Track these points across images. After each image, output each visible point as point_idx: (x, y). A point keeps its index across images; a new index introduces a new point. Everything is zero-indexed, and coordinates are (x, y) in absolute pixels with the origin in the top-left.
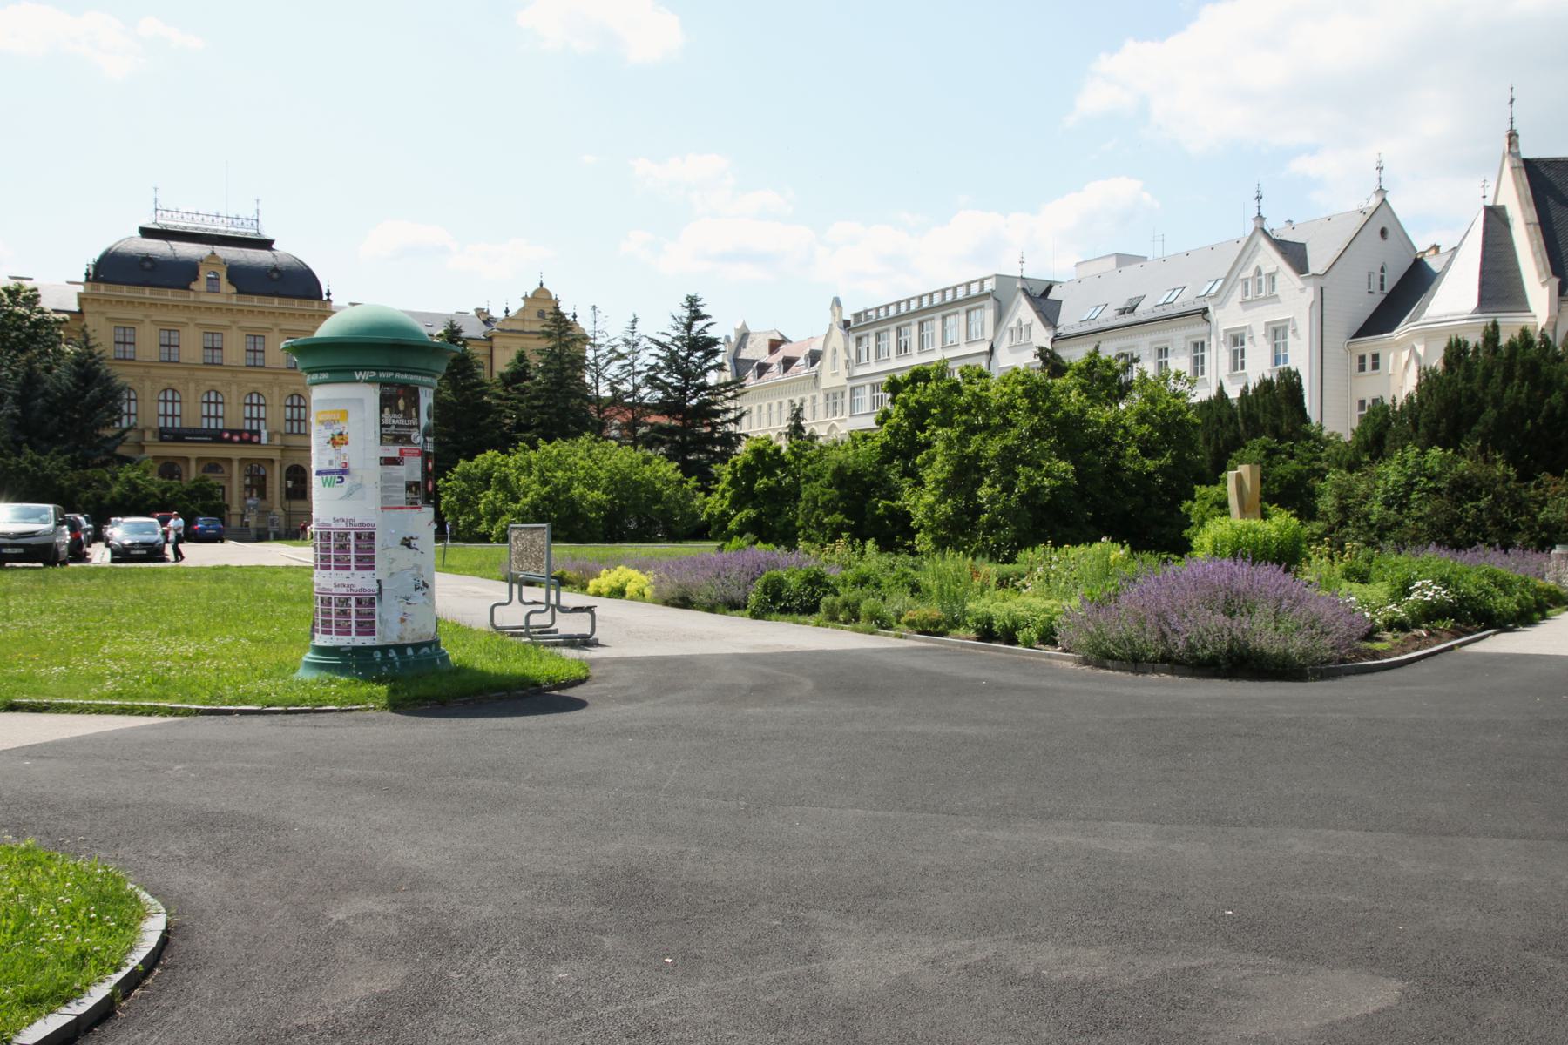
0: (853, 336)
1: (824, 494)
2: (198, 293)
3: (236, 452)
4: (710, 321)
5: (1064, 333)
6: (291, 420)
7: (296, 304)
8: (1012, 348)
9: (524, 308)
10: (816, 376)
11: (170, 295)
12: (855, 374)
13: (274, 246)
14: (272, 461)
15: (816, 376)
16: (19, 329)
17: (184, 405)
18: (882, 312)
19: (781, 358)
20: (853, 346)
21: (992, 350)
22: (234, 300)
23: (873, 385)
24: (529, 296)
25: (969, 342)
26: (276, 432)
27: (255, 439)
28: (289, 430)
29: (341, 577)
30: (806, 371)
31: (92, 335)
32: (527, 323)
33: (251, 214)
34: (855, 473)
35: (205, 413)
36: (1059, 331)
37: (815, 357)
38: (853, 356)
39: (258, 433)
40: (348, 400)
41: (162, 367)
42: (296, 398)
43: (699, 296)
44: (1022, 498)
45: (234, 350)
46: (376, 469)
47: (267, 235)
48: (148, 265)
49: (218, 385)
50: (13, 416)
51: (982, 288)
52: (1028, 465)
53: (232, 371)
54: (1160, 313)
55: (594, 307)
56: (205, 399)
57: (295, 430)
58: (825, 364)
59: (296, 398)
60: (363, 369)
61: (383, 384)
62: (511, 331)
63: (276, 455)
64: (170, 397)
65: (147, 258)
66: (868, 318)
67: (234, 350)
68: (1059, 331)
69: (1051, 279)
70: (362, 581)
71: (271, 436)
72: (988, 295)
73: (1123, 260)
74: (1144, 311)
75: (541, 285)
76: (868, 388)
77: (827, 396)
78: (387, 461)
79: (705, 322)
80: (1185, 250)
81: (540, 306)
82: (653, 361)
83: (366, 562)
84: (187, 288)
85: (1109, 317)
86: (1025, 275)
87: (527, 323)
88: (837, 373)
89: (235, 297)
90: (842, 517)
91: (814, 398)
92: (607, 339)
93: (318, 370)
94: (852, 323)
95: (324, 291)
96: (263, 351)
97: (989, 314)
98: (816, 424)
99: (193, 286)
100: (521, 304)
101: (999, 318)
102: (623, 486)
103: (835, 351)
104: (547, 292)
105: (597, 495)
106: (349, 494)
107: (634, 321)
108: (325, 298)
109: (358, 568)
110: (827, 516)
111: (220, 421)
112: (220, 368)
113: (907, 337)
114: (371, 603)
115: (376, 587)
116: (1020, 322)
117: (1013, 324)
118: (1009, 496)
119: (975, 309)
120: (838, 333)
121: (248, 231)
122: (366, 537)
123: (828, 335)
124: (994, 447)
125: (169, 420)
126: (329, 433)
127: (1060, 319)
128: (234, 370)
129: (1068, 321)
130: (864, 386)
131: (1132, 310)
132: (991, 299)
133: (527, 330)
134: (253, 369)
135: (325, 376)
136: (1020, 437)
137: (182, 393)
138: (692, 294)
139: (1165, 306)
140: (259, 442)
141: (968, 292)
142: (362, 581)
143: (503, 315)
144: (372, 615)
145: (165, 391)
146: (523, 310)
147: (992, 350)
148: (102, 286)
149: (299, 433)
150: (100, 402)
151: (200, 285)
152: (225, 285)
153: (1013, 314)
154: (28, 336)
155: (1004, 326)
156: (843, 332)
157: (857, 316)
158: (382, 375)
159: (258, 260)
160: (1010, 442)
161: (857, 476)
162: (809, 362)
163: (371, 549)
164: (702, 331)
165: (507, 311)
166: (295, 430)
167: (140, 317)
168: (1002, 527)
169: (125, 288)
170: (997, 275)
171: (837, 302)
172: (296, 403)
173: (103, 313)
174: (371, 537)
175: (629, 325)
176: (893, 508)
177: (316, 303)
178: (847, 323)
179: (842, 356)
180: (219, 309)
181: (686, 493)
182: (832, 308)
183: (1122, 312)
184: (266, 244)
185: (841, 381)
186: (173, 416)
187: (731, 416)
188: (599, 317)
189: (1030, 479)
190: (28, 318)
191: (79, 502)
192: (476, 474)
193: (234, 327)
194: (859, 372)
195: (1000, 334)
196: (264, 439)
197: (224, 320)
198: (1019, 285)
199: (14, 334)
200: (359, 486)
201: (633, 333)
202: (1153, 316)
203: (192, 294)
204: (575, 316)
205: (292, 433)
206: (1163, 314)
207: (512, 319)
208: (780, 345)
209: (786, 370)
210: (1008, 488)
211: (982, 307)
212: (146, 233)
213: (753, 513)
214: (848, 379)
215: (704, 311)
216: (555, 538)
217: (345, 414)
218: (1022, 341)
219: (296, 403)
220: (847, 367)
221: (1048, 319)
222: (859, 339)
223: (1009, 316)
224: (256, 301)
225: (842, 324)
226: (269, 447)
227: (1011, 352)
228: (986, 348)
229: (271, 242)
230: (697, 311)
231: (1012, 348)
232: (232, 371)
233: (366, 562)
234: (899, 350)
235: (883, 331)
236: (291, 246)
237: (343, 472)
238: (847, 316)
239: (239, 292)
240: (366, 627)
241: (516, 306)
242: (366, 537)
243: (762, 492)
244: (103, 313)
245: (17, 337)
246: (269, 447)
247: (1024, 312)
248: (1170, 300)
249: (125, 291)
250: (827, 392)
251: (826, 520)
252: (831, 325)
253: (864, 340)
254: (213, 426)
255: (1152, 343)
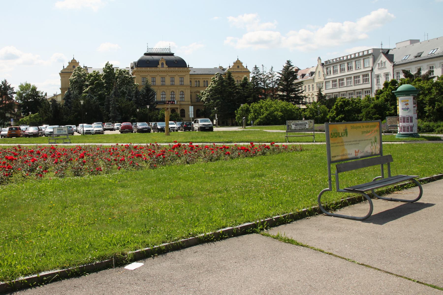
0: (325, 68)
1: (372, 110)
2: (159, 68)
3: (169, 106)
4: (293, 67)
5: (397, 64)
6: (181, 98)
7: (181, 69)
8: (379, 69)
9: (234, 65)
10: (313, 79)
11: (153, 69)
12: (326, 78)
13: (174, 55)
14: (177, 108)
15: (313, 79)
16: (127, 80)
17: (166, 95)
18: (334, 60)
19: (301, 74)
20: (325, 70)
21: (372, 70)
22: (167, 69)
23: (332, 81)
24: (70, 62)
25: (364, 67)
26: (179, 101)
27: (174, 103)
28: (180, 100)
29: (408, 124)
30: (310, 78)
31: (148, 80)
32: (235, 69)
33: (168, 47)
34: (380, 105)
35: (162, 97)
36: (395, 63)
37: (312, 74)
38: (325, 73)
39: (174, 101)
40: (409, 99)
41: (162, 86)
42: (182, 92)
43: (290, 60)
44: (437, 109)
45: (168, 81)
46: (413, 108)
47: (172, 52)
48: (148, 62)
49: (164, 90)
50: (135, 100)
51: (368, 53)
52: (438, 102)
53: (186, 86)
54: (430, 56)
55: (263, 65)
56: (180, 94)
57: (182, 100)
58: (316, 76)
59: (182, 92)
60: (411, 94)
61: (413, 96)
62: (65, 72)
63: (178, 107)
64: (173, 93)
65: (148, 61)
66: (330, 62)
67: (168, 81)
68: (395, 63)
69: (389, 48)
70: (411, 124)
71: (177, 102)
72: (370, 54)
73: (413, 42)
74: (423, 56)
75: (238, 59)
76: (331, 82)
77: (317, 84)
78: (414, 107)
79: (292, 67)
80: (437, 37)
81: (238, 65)
82: (277, 78)
83: (411, 121)
84: (157, 67)
85: (412, 58)
86: (383, 48)
87: (235, 69)
88: (320, 78)
89: (167, 68)
90: (378, 116)
91: (313, 85)
92: (266, 73)
93: (399, 95)
94: (325, 64)
95: (187, 65)
96: (183, 81)
97: (371, 60)
98: (314, 92)
99: (158, 66)
100: (68, 64)
101: (374, 61)
102: (284, 110)
103: (319, 72)
104: (240, 61)
105: (280, 114)
106: (409, 112)
107: (272, 68)
108: (188, 67)
109: (410, 122)
110: (373, 115)
111: (165, 99)
112: (174, 86)
113: (343, 67)
114: (412, 127)
115: (413, 125)
116: (381, 61)
117: (379, 62)
118: (433, 109)
119: (366, 58)
120: (320, 68)
121: (167, 51)
122: (411, 118)
123: (317, 67)
124: (427, 98)
125: (163, 99)
126: (405, 103)
127: (394, 60)
128: (177, 86)
129: (397, 60)
130: (330, 81)
131: (420, 56)
132: (371, 56)
133: (235, 71)
134: (181, 86)
135: (405, 95)
136: (435, 96)
137: (175, 93)
138: (288, 60)
139: (432, 54)
140: (175, 104)
141: (363, 54)
142: (411, 124)
143: (228, 68)
144: (412, 129)
145: (172, 92)
146: (233, 66)
147: (372, 70)
148: (139, 68)
149: (183, 101)
150: (151, 95)
151: (160, 66)
152: (165, 66)
153: (380, 58)
154: (128, 81)
155: (376, 62)
156: (322, 66)
157: (326, 62)
158: (414, 95)
159: (172, 59)
160: (432, 97)
161: (380, 106)
162: (310, 75)
163: (412, 120)
164: (291, 69)
165: (64, 67)
166: (182, 100)
167: (147, 75)
168: (432, 116)
169: (144, 68)
170: (373, 49)
171: (319, 58)
172: (163, 94)
173: (139, 75)
174: (412, 118)
175: (271, 69)
176: (391, 113)
177: (186, 68)
178: (323, 64)
179: (322, 73)
180: (164, 72)
181: (300, 112)
182: (318, 60)
183: (416, 57)
184: (172, 54)
185: (322, 79)
186: (164, 98)
187: (300, 91)
188: (264, 67)
189: (439, 105)
190: (128, 77)
191: (152, 119)
192: (244, 109)
193: (168, 76)
194: (328, 77)
195: (375, 65)
196: (176, 103)
197: (146, 74)
198: (381, 51)
199: (126, 81)
200: (411, 111)
201: (272, 71)
202: (428, 57)
203: (158, 68)
204: (247, 67)
205: (181, 101)
206: (431, 57)
207: (231, 69)
208: (298, 71)
209: (303, 78)
210: (433, 107)
211: (369, 58)
212: (146, 54)
213: (343, 116)
214: (324, 79)
215: (292, 64)
216: (315, 123)
217: (408, 101)
218: (383, 67)
219: (163, 94)
220: (324, 76)
221: (391, 60)
222: (327, 68)
223: (378, 60)
224: (172, 69)
225: (321, 64)
226: (177, 105)
227: (379, 70)
228: (370, 69)
229: (174, 54)
230: (290, 64)
231: (379, 69)
232: (186, 86)
233: (411, 121)
234: (341, 71)
235: (335, 66)
236: (178, 54)
237: (408, 109)
238: (323, 62)
239: (168, 67)
240: (412, 131)
241: (232, 65)
242: (411, 118)
243: (347, 110)
244: (139, 75)
245: (126, 82)
246: (177, 105)
247: (383, 58)
248: (433, 52)
249: (144, 69)
250: (317, 83)
251: (373, 117)
252: (318, 65)
253: (329, 69)
254: (163, 100)
255: (428, 65)
